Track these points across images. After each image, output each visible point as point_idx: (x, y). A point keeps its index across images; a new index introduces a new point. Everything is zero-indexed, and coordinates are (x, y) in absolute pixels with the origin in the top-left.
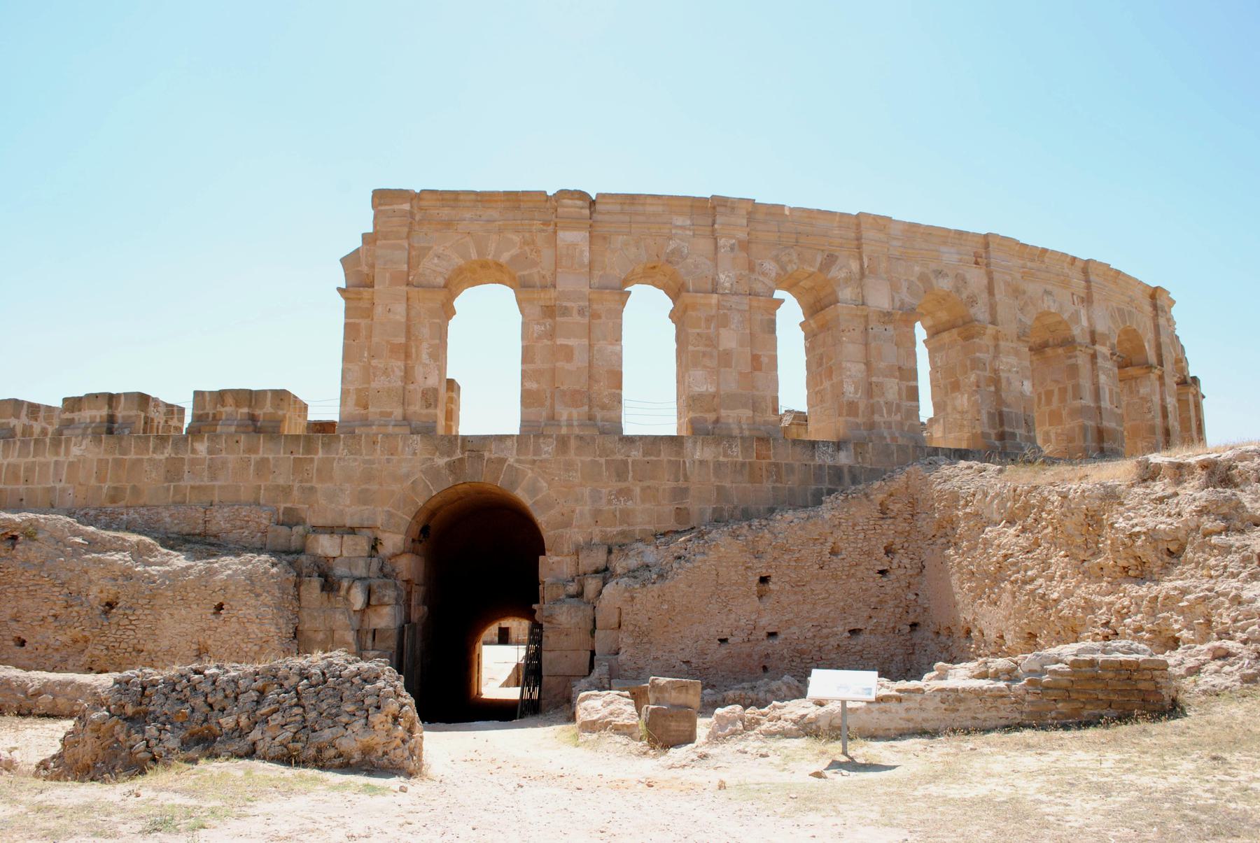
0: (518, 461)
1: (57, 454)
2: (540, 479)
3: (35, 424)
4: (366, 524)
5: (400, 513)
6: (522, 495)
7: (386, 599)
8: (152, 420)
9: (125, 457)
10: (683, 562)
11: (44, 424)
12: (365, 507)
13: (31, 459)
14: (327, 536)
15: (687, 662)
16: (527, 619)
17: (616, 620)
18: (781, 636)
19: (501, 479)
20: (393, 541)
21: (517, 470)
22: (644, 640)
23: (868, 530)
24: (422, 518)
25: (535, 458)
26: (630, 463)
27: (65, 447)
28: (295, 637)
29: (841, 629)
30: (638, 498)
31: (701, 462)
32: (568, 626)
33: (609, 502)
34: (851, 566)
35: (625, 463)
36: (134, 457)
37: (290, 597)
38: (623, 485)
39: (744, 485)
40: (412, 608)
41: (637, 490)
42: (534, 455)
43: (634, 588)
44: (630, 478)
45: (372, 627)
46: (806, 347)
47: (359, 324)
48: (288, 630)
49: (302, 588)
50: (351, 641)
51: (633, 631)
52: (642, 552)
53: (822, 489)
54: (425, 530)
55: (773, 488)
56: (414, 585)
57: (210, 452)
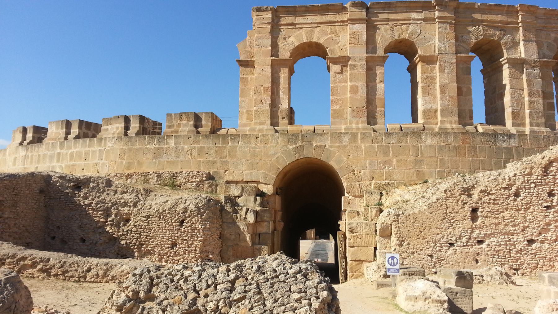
0: (331, 147)
1: (100, 146)
3: (175, 124)
5: (270, 174)
6: (333, 163)
7: (265, 218)
8: (146, 129)
9: (133, 147)
11: (94, 132)
13: (87, 149)
14: (234, 185)
20: (268, 189)
21: (330, 151)
23: (537, 182)
24: (281, 176)
27: (104, 142)
28: (220, 238)
29: (522, 239)
34: (527, 204)
36: (138, 147)
37: (217, 217)
38: (387, 158)
40: (277, 223)
42: (339, 143)
45: (258, 232)
46: (484, 83)
47: (247, 78)
57: (175, 144)
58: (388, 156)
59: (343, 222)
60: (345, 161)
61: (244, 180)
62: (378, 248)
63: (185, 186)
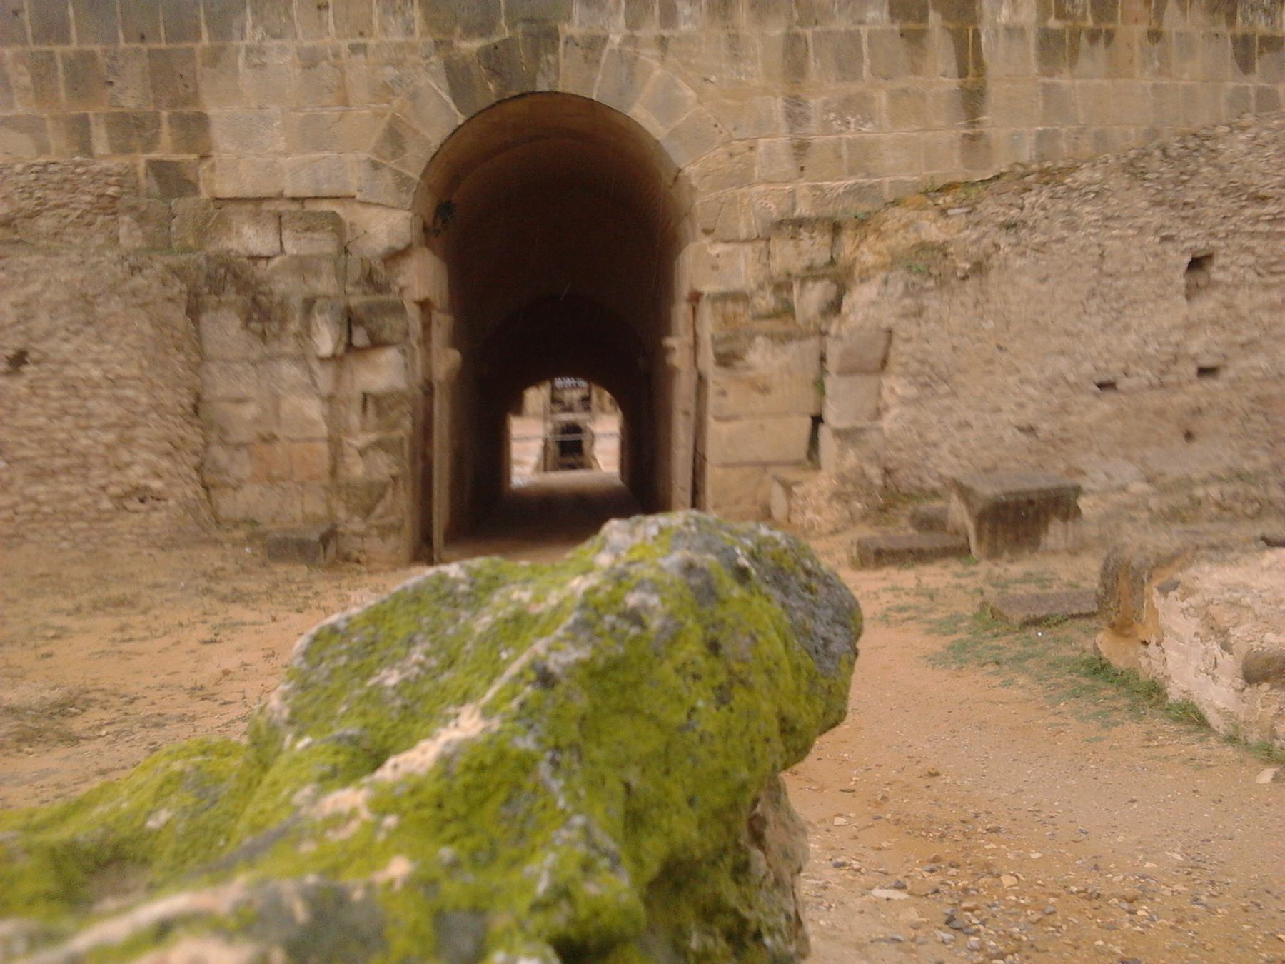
2: (679, 81)
4: (326, 190)
6: (641, 113)
10: (1023, 232)
12: (315, 155)
15: (1030, 430)
17: (878, 354)
18: (1228, 374)
19: (597, 83)
25: (666, 33)
26: (865, 39)
31: (1009, 30)
33: (826, 126)
35: (854, 38)
38: (854, 88)
39: (1098, 81)
41: (882, 99)
43: (922, 288)
49: (204, 319)
53: (1247, 88)
55: (1155, 87)
58: (856, 76)
59: (688, 339)
61: (288, 193)
63: (689, 916)
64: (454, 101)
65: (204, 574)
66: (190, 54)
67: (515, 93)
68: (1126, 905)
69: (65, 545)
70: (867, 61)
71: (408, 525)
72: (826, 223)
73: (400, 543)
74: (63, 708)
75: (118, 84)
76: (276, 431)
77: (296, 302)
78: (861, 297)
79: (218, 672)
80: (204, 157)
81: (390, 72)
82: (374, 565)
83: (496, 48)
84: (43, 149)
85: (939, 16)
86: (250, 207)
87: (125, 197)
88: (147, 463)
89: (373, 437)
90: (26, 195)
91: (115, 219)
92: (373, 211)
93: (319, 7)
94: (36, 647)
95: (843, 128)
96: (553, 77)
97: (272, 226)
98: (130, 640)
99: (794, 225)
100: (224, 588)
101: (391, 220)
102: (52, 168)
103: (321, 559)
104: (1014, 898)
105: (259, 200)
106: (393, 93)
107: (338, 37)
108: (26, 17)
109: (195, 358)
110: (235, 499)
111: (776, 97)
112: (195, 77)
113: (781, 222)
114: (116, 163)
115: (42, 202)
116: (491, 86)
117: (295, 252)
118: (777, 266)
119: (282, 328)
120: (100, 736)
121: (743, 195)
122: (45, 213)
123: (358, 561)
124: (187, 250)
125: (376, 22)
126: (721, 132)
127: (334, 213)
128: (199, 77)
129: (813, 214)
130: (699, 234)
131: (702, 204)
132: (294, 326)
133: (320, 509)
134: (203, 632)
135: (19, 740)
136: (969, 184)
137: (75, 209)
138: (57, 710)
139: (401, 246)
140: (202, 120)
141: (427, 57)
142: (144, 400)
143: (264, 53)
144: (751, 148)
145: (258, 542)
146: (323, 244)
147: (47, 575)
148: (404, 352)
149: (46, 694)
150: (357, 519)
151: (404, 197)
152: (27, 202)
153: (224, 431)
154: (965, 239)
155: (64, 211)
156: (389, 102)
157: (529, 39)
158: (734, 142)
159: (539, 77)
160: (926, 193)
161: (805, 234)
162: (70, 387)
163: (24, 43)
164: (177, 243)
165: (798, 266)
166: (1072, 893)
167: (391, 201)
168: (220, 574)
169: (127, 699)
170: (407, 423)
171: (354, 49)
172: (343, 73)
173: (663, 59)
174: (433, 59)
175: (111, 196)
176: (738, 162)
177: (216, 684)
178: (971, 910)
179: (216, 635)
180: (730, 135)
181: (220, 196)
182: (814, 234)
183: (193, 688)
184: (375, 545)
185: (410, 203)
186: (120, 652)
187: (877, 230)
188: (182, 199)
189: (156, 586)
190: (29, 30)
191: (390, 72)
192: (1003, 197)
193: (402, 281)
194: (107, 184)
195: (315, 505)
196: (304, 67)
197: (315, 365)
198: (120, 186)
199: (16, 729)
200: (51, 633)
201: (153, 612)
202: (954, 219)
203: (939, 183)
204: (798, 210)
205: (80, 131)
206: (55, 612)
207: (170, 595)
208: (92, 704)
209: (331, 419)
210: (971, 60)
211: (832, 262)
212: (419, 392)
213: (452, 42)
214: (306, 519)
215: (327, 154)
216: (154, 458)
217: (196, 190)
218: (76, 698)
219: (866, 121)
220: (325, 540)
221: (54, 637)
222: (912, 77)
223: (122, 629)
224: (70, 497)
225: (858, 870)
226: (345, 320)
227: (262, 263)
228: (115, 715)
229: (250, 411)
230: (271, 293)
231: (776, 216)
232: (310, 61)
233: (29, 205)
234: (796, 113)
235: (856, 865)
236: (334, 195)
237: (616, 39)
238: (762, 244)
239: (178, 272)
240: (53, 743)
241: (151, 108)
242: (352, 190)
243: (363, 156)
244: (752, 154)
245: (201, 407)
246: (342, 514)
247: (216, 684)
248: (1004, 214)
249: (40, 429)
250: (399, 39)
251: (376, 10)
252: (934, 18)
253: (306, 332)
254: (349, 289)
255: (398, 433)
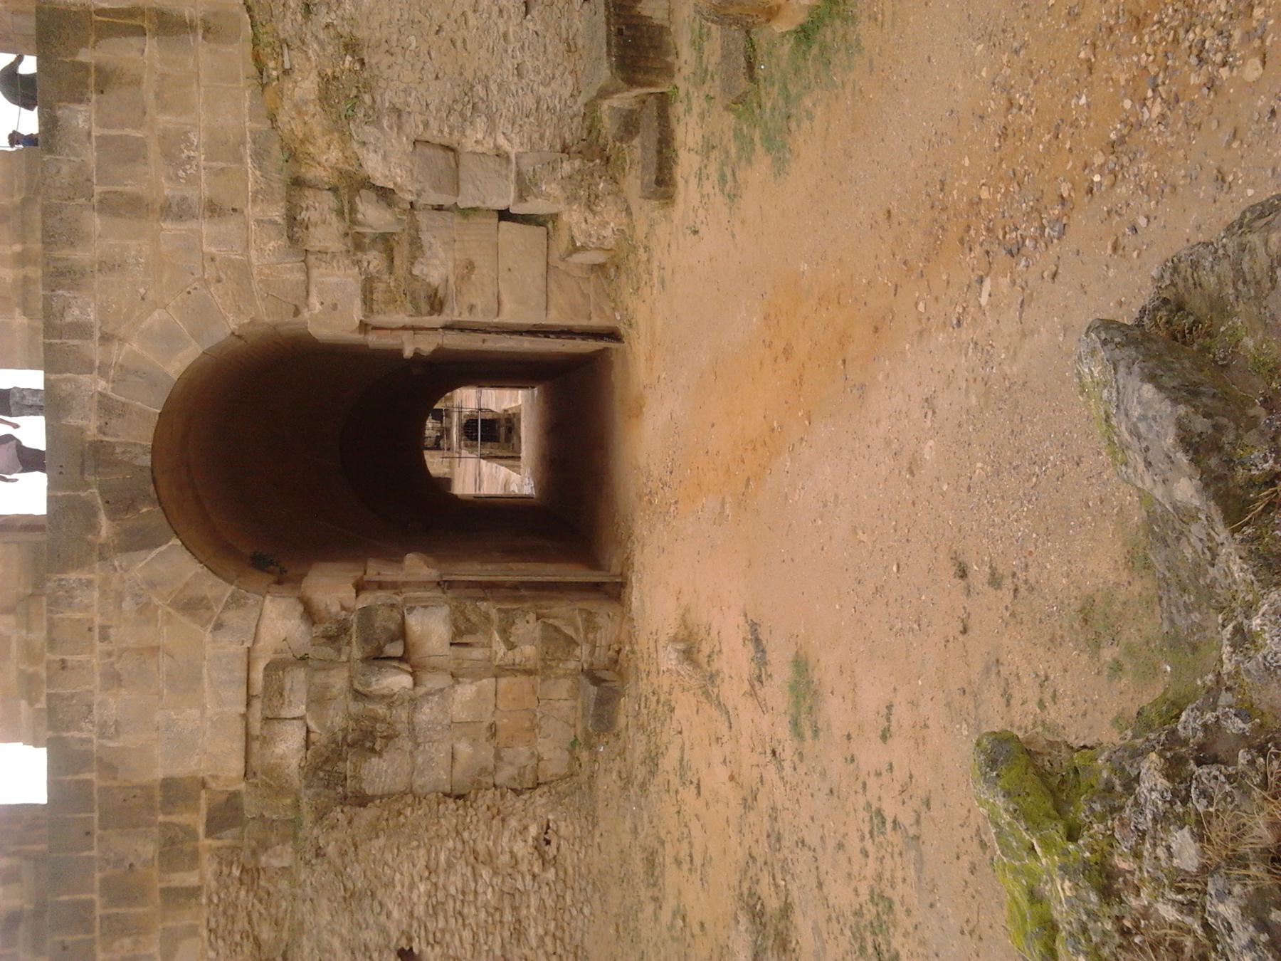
6: (176, 365)
12: (206, 681)
16: (456, 497)
22: (482, 93)
25: (97, 334)
26: (106, 132)
30: (183, 119)
32: (451, 264)
33: (192, 181)
35: (104, 142)
38: (154, 150)
41: (166, 120)
44: (139, 135)
48: (450, 811)
49: (369, 792)
50: (474, 688)
51: (462, 115)
52: (296, 106)
54: (260, 563)
56: (366, 578)
59: (406, 335)
60: (166, 316)
61: (242, 709)
62: (502, 205)
64: (157, 546)
65: (624, 788)
66: (105, 791)
67: (152, 488)
68: (1015, 111)
69: (586, 911)
70: (128, 131)
71: (584, 605)
72: (293, 193)
73: (604, 612)
74: (757, 915)
75: (132, 859)
76: (486, 724)
77: (356, 708)
78: (375, 167)
79: (729, 785)
80: (204, 784)
81: (128, 604)
82: (624, 636)
83: (107, 502)
84: (193, 931)
85: (83, 50)
86: (256, 746)
87: (241, 860)
88: (513, 838)
89: (496, 636)
90: (239, 949)
91: (263, 869)
92: (263, 631)
93: (63, 668)
94: (693, 936)
95: (194, 163)
96: (138, 450)
97: (277, 726)
98: (691, 856)
99: (294, 225)
100: (640, 773)
101: (273, 616)
102: (213, 925)
103: (617, 685)
104: (999, 196)
105: (248, 737)
106: (148, 604)
107: (92, 651)
108: (69, 939)
109: (409, 799)
110: (550, 760)
111: (162, 229)
112: (128, 788)
113: (290, 238)
114: (209, 867)
115: (245, 935)
116: (145, 510)
117: (304, 707)
118: (335, 245)
119: (384, 720)
120: (785, 886)
121: (260, 273)
122: (256, 933)
123: (618, 652)
124: (296, 806)
125: (78, 615)
126: (196, 289)
127: (265, 669)
128: (127, 784)
129: (282, 204)
130: (300, 319)
131: (268, 315)
132: (381, 710)
133: (566, 684)
134: (688, 794)
135: (785, 950)
136: (255, 41)
137: (253, 905)
138: (758, 920)
139: (300, 608)
140: (168, 784)
141: (115, 569)
142: (450, 844)
143: (105, 722)
144: (213, 259)
145: (594, 740)
146: (296, 680)
147: (617, 925)
148: (411, 609)
149: (742, 928)
150: (578, 652)
151: (251, 602)
152: (245, 949)
153: (483, 771)
154: (318, 56)
155: (255, 916)
156: (157, 608)
157: (100, 470)
158: (206, 277)
159: (137, 462)
160: (263, 86)
161: (304, 215)
162: (435, 910)
163: (93, 941)
164: (289, 813)
165: (336, 225)
166: (1000, 147)
167: (255, 615)
168: (624, 775)
169: (750, 862)
170: (483, 606)
171: (104, 637)
172: (126, 649)
173: (122, 340)
174: (116, 563)
175: (242, 872)
176: (226, 274)
177: (742, 787)
178: (1005, 233)
179: (691, 782)
180: (198, 280)
181: (243, 772)
182: (304, 205)
183: (745, 807)
184: (603, 637)
185: (258, 597)
186: (703, 865)
187: (302, 142)
188: (246, 807)
189: (635, 831)
190: (80, 937)
191: (128, 604)
192: (276, 12)
193: (335, 608)
194: (230, 874)
195: (560, 690)
196: (120, 686)
197: (421, 690)
198: (232, 863)
199: (775, 953)
200: (680, 923)
201: (663, 834)
202: (294, 62)
203: (253, 70)
204: (277, 218)
205: (178, 897)
206: (656, 919)
207: (646, 819)
208: (753, 891)
209: (475, 675)
210: (127, 21)
211: (334, 190)
212: (450, 594)
213: (100, 544)
214: (575, 698)
215: (205, 671)
216: (507, 834)
217: (236, 795)
218: (748, 905)
219: (188, 140)
220: (596, 681)
221: (684, 920)
222: (144, 87)
223: (678, 863)
224: (542, 907)
225: (964, 308)
226: (376, 662)
227: (313, 737)
228: (765, 872)
229: (464, 748)
230: (345, 730)
231: (283, 242)
232: (113, 679)
233: (248, 947)
234: (177, 211)
235: (959, 309)
236: (245, 667)
237: (102, 385)
238: (312, 258)
239: (321, 815)
240: (789, 924)
241: (155, 830)
242: (242, 650)
243: (208, 637)
244: (218, 259)
245: (456, 793)
246: (572, 665)
247: (742, 787)
248: (294, 13)
249: (474, 935)
250: (96, 594)
251: (68, 614)
252: (85, 56)
253: (388, 699)
254: (344, 658)
255: (494, 614)
